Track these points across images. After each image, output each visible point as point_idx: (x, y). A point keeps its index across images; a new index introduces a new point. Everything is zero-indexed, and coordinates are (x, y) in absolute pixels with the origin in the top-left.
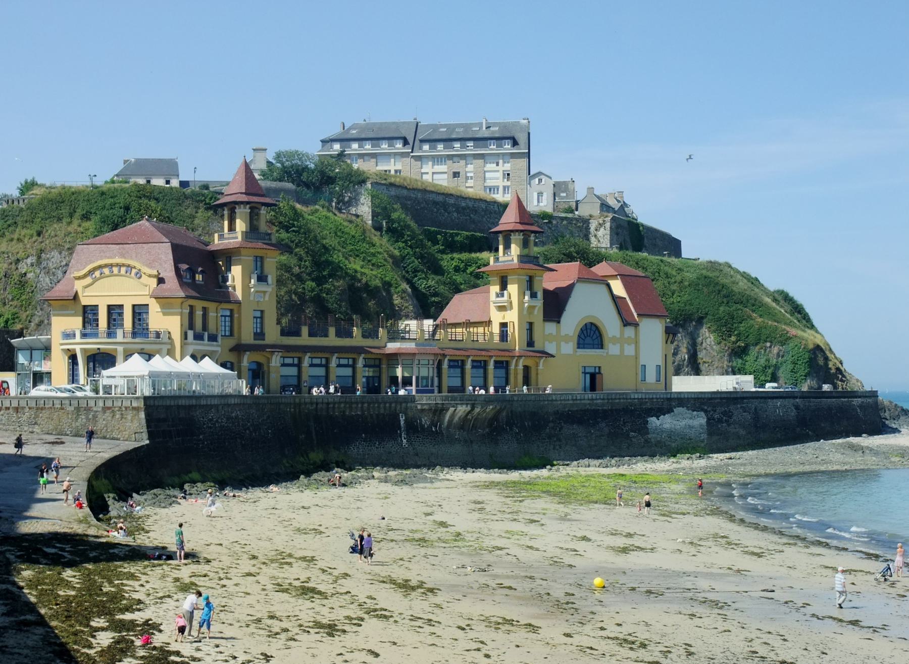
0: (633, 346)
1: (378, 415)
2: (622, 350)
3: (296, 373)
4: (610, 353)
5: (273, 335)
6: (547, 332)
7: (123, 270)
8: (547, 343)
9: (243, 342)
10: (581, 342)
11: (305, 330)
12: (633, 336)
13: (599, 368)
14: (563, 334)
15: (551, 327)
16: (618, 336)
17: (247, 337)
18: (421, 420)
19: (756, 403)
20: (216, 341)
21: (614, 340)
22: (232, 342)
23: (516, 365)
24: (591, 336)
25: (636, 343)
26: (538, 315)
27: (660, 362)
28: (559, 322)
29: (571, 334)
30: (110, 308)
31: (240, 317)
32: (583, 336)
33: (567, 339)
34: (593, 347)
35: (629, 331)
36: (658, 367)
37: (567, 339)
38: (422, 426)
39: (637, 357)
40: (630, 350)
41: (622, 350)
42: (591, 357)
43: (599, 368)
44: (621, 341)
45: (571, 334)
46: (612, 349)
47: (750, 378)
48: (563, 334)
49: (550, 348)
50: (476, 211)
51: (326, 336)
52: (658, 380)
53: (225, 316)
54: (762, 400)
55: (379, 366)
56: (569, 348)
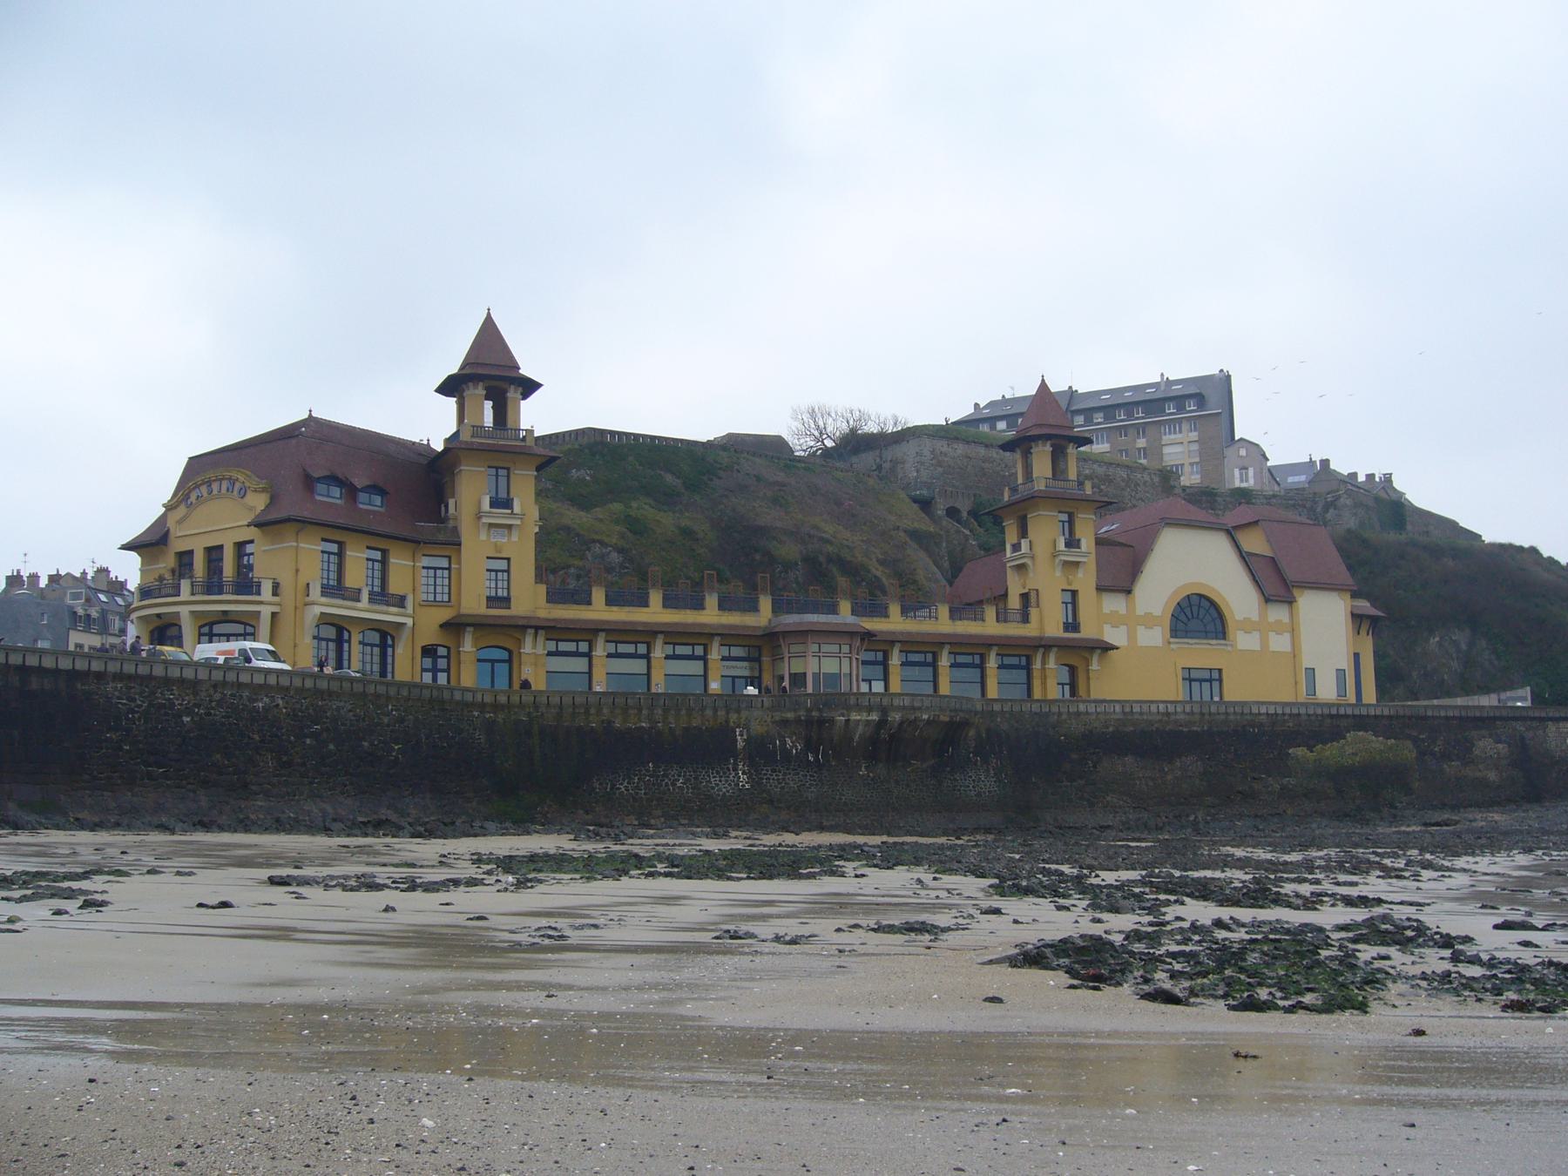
0: (1287, 636)
1: (686, 730)
2: (1264, 642)
3: (586, 669)
4: (1240, 647)
5: (529, 599)
6: (1106, 610)
7: (225, 484)
8: (1107, 628)
9: (464, 611)
10: (1181, 626)
11: (598, 595)
12: (1286, 619)
13: (1220, 671)
14: (1140, 611)
15: (1114, 604)
16: (1255, 617)
17: (473, 602)
18: (783, 743)
19: (1520, 727)
20: (403, 607)
21: (1247, 626)
22: (445, 615)
23: (1044, 663)
24: (1198, 616)
25: (1293, 630)
26: (1085, 581)
27: (1345, 663)
28: (1129, 592)
29: (1157, 612)
30: (209, 550)
31: (459, 570)
32: (1183, 617)
33: (1149, 621)
34: (1205, 634)
35: (1278, 613)
36: (1341, 673)
37: (1149, 621)
38: (786, 753)
39: (1295, 654)
40: (1280, 643)
41: (1264, 642)
42: (1201, 654)
43: (1220, 671)
44: (1262, 628)
45: (1157, 612)
46: (1245, 641)
47: (908, 552)
48: (1140, 611)
49: (1112, 636)
50: (1111, 481)
51: (644, 603)
52: (1342, 690)
53: (330, 553)
54: (1535, 724)
55: (758, 660)
56: (1154, 637)
